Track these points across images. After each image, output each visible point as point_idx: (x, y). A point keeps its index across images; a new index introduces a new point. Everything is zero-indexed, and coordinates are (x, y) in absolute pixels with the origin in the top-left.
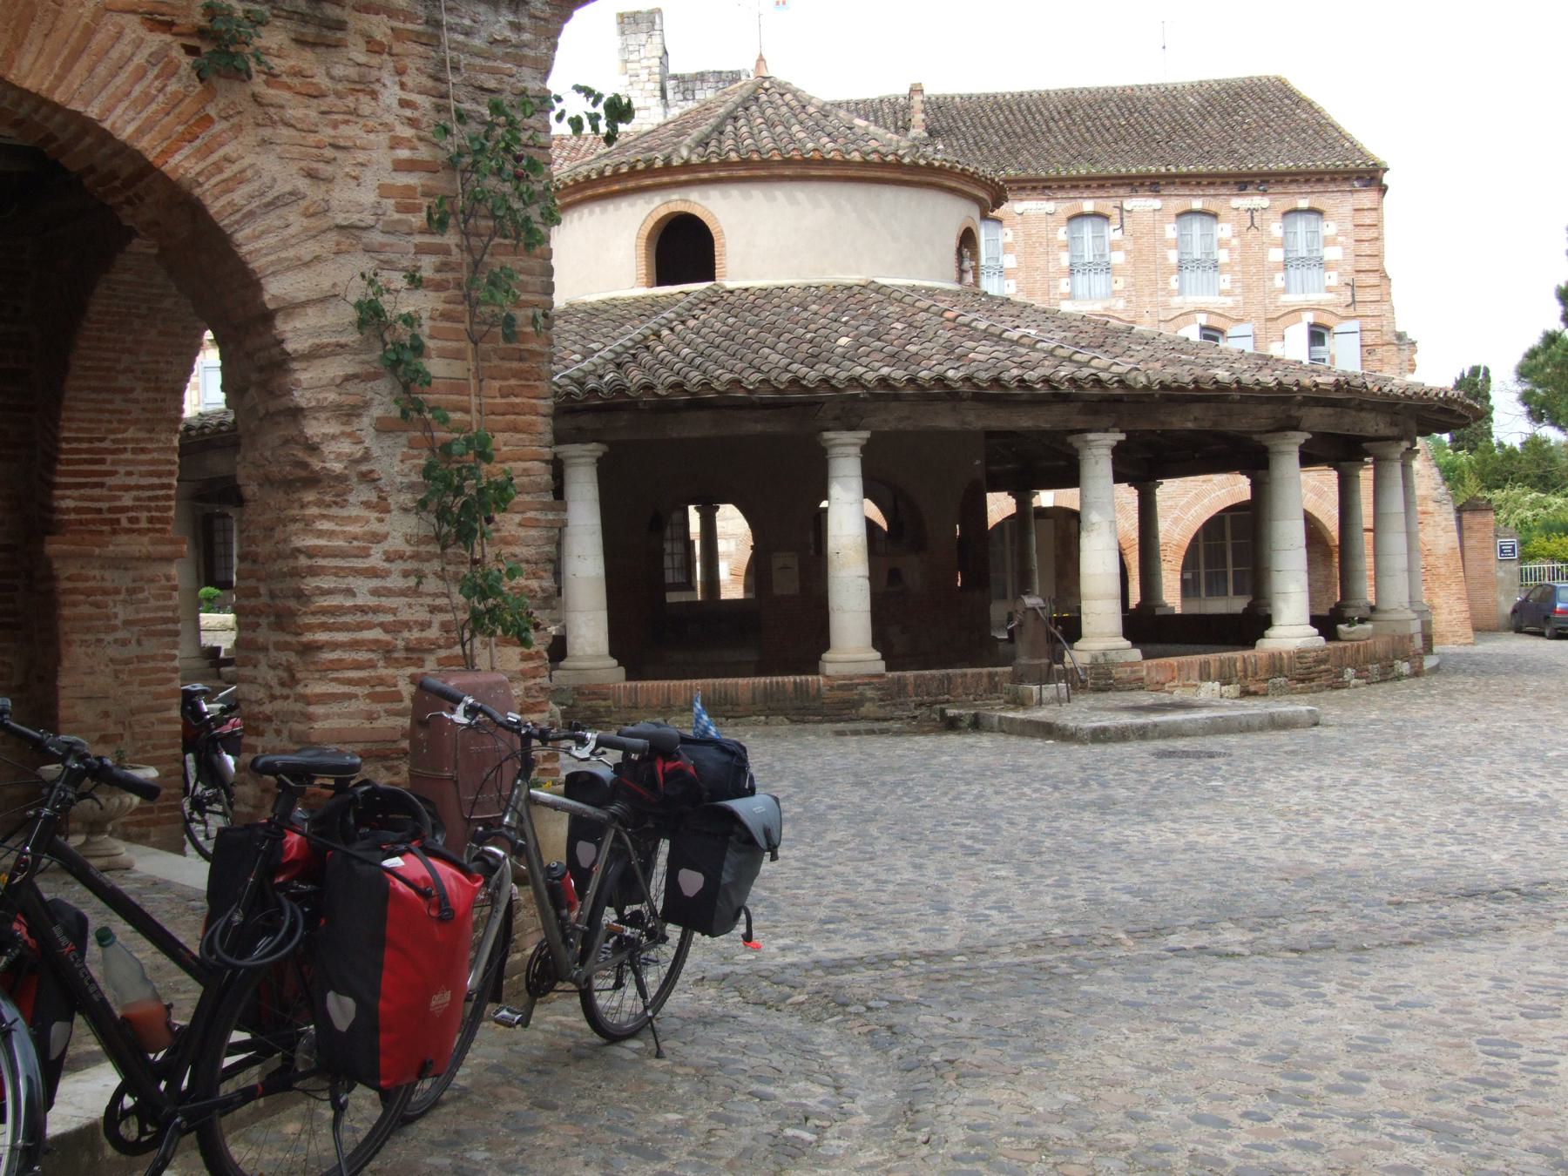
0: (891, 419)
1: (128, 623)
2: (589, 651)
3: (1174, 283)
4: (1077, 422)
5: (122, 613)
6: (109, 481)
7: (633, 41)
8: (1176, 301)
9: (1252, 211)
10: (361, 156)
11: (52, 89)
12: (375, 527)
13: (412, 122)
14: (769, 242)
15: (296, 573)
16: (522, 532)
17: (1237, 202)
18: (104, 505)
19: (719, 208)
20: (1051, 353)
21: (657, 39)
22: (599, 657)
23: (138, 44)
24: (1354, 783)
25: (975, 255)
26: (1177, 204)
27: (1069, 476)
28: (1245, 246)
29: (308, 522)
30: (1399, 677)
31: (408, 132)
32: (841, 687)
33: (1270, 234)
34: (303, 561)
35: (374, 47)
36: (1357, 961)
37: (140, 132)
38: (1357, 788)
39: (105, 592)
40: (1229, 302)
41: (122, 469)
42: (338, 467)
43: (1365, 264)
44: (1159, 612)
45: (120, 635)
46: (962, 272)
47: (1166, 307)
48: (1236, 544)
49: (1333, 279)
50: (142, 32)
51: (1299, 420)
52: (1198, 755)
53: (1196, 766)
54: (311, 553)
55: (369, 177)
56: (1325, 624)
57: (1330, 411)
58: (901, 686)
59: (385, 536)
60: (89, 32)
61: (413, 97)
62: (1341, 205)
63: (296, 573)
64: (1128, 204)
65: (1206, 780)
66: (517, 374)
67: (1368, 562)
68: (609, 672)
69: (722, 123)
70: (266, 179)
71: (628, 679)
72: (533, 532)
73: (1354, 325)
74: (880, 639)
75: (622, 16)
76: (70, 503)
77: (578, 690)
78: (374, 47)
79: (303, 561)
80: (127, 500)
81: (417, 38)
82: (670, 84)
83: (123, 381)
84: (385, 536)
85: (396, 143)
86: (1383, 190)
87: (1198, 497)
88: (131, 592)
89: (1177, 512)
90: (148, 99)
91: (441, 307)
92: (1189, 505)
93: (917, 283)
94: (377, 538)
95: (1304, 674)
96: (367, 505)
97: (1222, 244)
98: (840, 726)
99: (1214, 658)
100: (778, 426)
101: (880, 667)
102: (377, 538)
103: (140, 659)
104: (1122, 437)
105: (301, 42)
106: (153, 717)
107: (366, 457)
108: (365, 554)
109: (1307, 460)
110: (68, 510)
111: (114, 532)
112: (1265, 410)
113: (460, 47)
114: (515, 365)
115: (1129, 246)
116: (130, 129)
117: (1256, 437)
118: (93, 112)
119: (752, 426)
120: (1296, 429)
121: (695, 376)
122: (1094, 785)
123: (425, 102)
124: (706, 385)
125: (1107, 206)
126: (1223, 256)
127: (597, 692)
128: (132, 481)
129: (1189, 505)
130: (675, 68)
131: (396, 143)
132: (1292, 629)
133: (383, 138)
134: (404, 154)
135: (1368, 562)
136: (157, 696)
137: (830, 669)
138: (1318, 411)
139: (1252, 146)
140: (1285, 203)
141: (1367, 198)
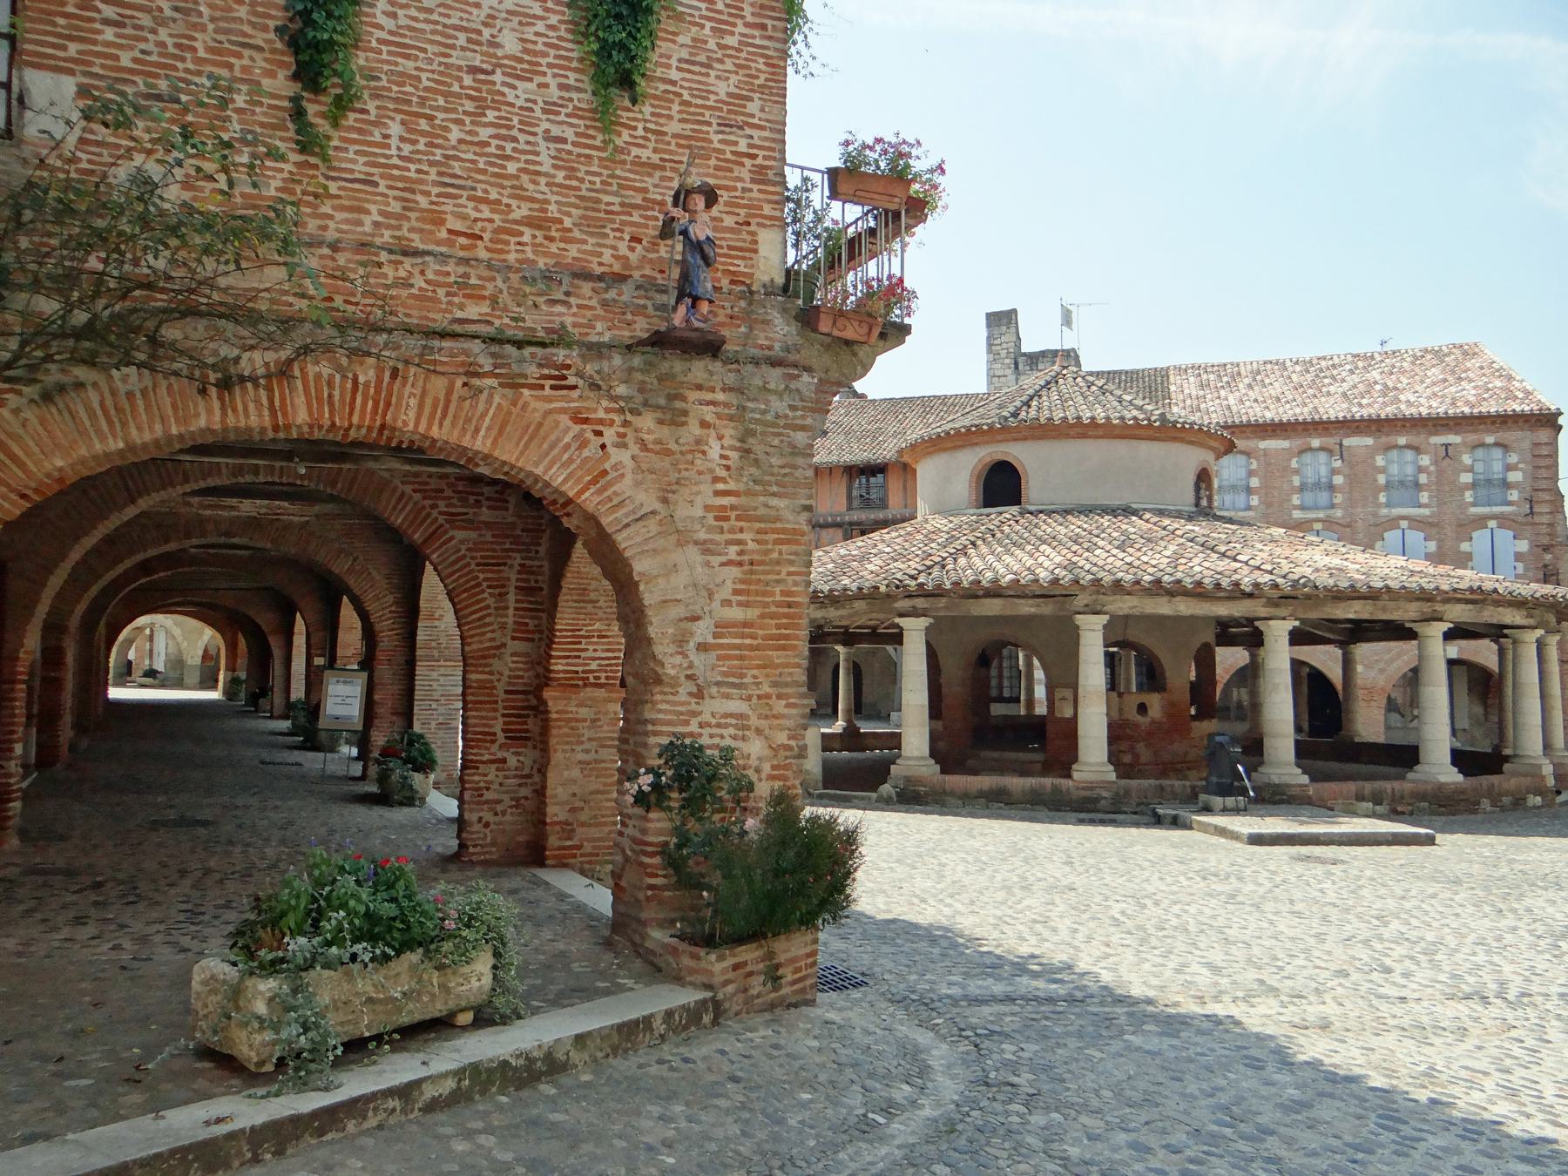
0: (1123, 605)
1: (590, 740)
2: (916, 753)
3: (1382, 498)
4: (1262, 611)
5: (587, 734)
6: (583, 654)
7: (996, 331)
9: (1447, 446)
10: (695, 489)
11: (518, 459)
12: (694, 707)
13: (728, 468)
15: (646, 734)
16: (786, 711)
17: (1435, 440)
18: (580, 669)
19: (1020, 454)
20: (1246, 563)
21: (1013, 330)
22: (923, 758)
23: (567, 430)
24: (1434, 896)
25: (1209, 487)
28: (1440, 472)
29: (654, 703)
30: (1527, 809)
31: (723, 473)
32: (1083, 788)
33: (1461, 462)
34: (650, 727)
35: (704, 424)
37: (565, 481)
38: (1433, 901)
39: (578, 720)
40: (1426, 511)
41: (591, 648)
42: (673, 672)
43: (1543, 485)
44: (1357, 740)
45: (587, 746)
46: (1198, 499)
47: (1375, 515)
49: (1514, 495)
50: (570, 423)
51: (1443, 613)
52: (1321, 861)
53: (1319, 870)
54: (654, 722)
55: (699, 501)
56: (1460, 759)
57: (1470, 606)
59: (700, 713)
60: (540, 425)
61: (728, 453)
63: (646, 734)
64: (1346, 442)
65: (1320, 882)
66: (786, 616)
68: (930, 770)
69: (1031, 398)
70: (637, 503)
71: (943, 772)
72: (794, 711)
74: (1114, 758)
75: (989, 316)
76: (560, 668)
78: (704, 424)
79: (650, 727)
80: (594, 666)
81: (731, 418)
82: (1021, 360)
83: (593, 596)
84: (700, 713)
85: (716, 480)
87: (1399, 655)
88: (594, 721)
89: (1381, 665)
90: (570, 460)
91: (740, 576)
92: (1392, 660)
94: (694, 714)
96: (690, 694)
97: (1297, 472)
98: (1083, 815)
99: (1368, 787)
100: (1047, 609)
101: (1113, 776)
102: (694, 714)
103: (596, 761)
104: (1297, 623)
105: (661, 422)
106: (600, 796)
107: (691, 667)
108: (687, 723)
110: (559, 672)
111: (585, 685)
112: (1415, 606)
113: (758, 422)
114: (786, 610)
115: (1347, 472)
116: (560, 480)
117: (1408, 625)
118: (538, 471)
119: (1027, 608)
120: (1440, 620)
121: (989, 575)
122: (1233, 879)
123: (734, 455)
124: (995, 581)
126: (1423, 479)
127: (919, 781)
128: (597, 655)
129: (1392, 660)
130: (1025, 349)
131: (716, 480)
133: (708, 477)
134: (721, 486)
136: (605, 785)
137: (1076, 775)
138: (1460, 607)
141: (1543, 435)
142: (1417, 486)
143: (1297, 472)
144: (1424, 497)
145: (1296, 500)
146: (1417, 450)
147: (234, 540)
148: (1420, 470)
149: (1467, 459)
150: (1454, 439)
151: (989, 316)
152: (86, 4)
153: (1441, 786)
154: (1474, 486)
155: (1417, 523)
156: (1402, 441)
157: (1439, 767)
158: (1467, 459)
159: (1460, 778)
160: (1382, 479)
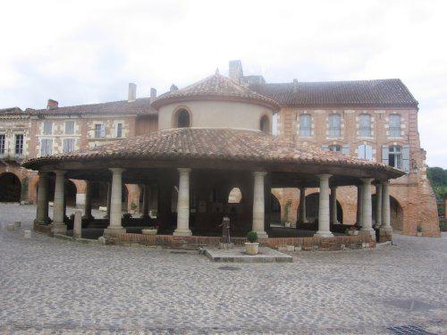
8: (358, 138)
14: (204, 119)
26: (359, 112)
27: (317, 184)
36: (406, 305)
48: (311, 204)
49: (403, 133)
56: (333, 228)
58: (194, 240)
62: (405, 113)
64: (345, 111)
67: (380, 209)
73: (408, 146)
77: (110, 235)
86: (418, 109)
93: (205, 128)
95: (324, 245)
97: (327, 122)
109: (373, 183)
124: (113, 154)
125: (340, 112)
132: (325, 232)
135: (380, 209)
139: (392, 98)
140: (389, 112)
141: (413, 111)
142: (370, 129)
143: (327, 122)
144: (373, 133)
145: (327, 133)
146: (370, 115)
147: (263, 256)
148: (371, 123)
149: (357, 119)
150: (382, 112)
151: (240, 61)
152: (4, 319)
153: (324, 239)
154: (389, 129)
155: (370, 143)
156: (305, 112)
157: (325, 232)
158: (387, 119)
159: (332, 236)
160: (358, 126)
